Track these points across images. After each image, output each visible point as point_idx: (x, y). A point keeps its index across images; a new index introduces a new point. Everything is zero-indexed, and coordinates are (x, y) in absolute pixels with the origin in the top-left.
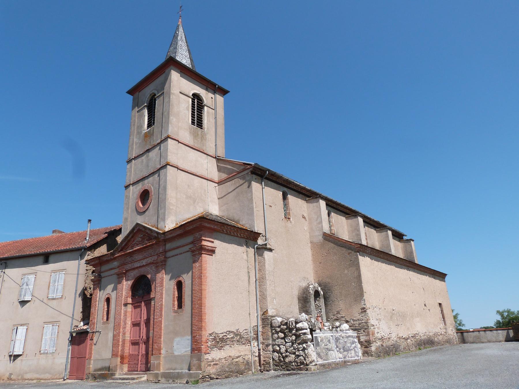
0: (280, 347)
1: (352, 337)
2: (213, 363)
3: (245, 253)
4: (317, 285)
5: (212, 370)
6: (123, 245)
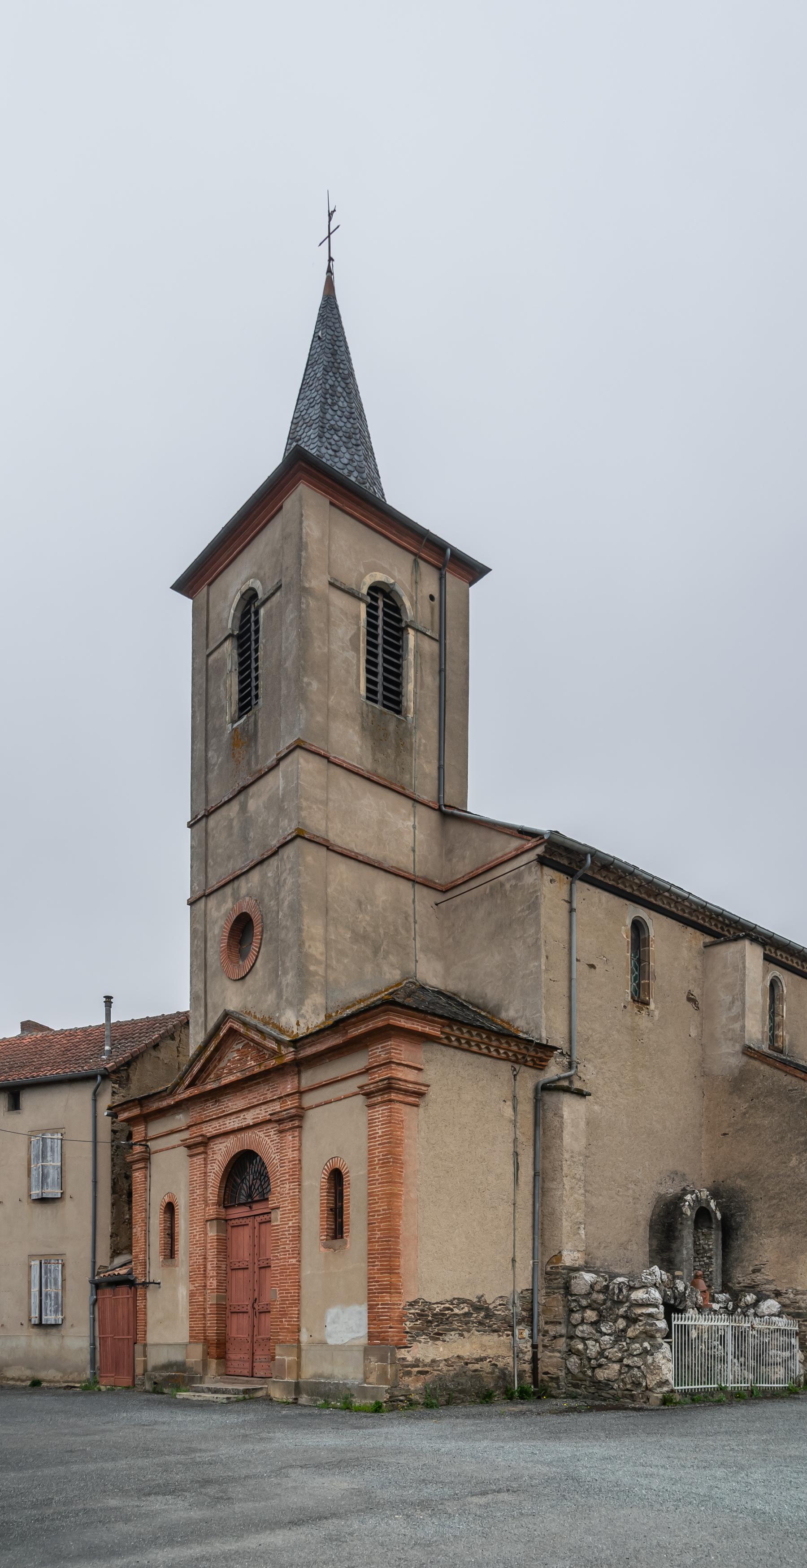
0: (585, 1344)
1: (784, 1332)
2: (417, 1369)
3: (509, 1103)
4: (705, 1194)
5: (414, 1385)
6: (196, 1070)
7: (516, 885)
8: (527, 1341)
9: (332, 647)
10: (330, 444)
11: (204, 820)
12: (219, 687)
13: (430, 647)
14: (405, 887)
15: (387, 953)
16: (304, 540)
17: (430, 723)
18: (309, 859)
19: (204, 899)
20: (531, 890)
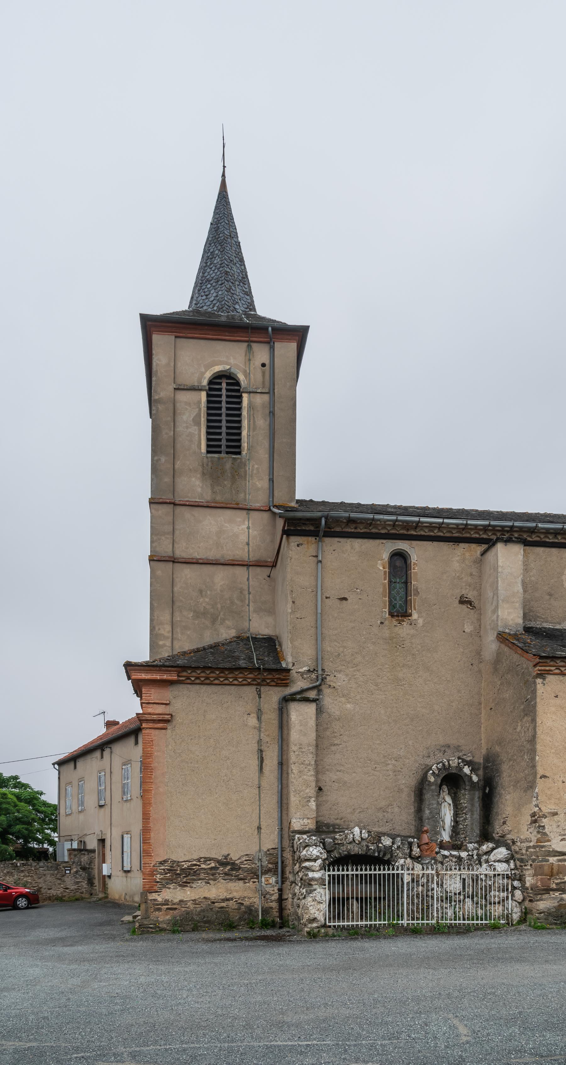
5: (163, 917)
8: (273, 886)
14: (240, 572)
15: (223, 620)
17: (262, 453)
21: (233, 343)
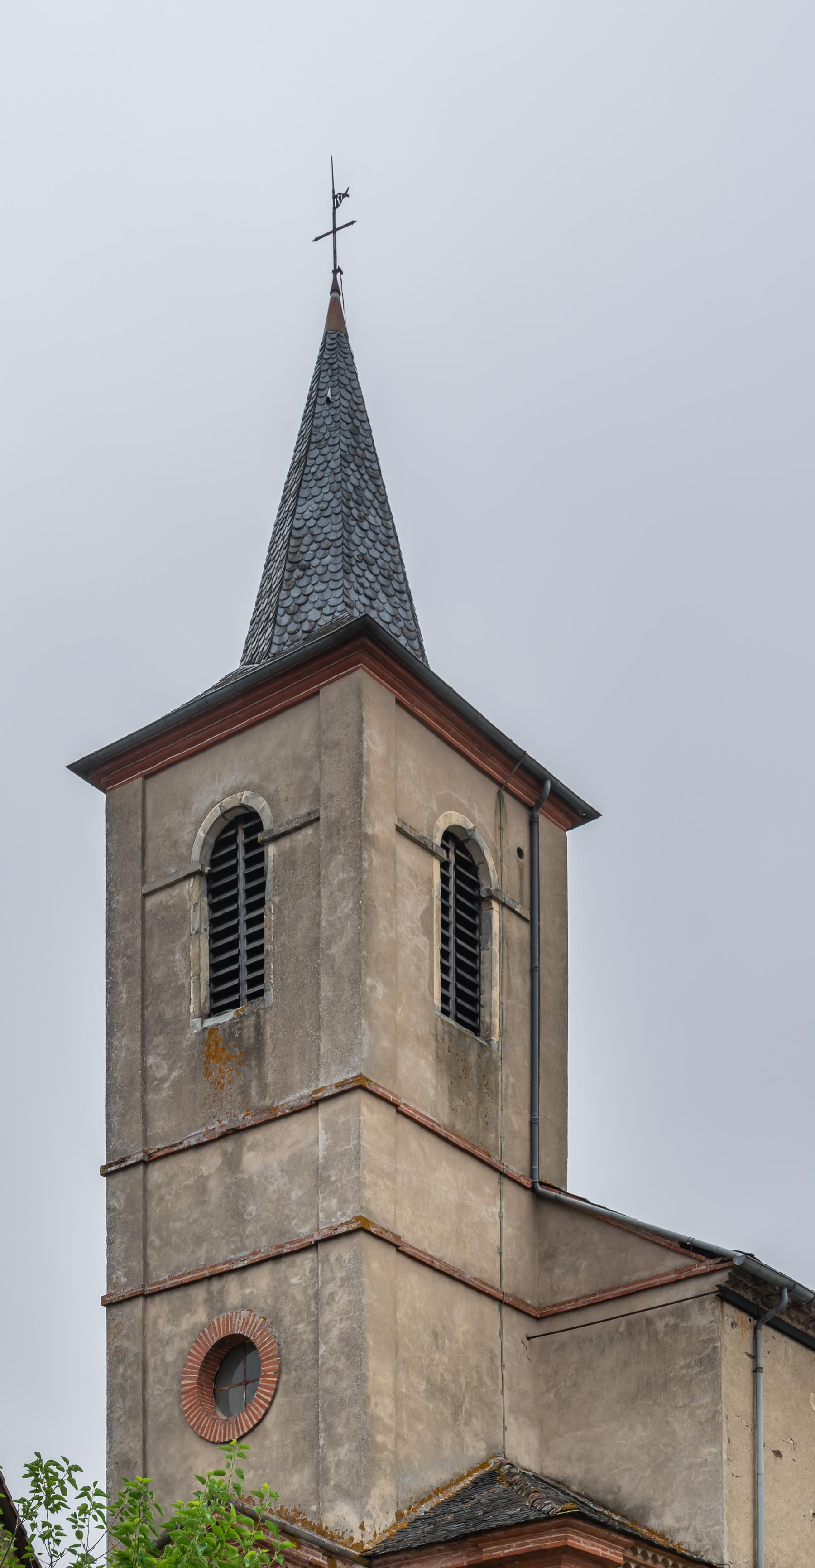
7: (676, 1326)
9: (399, 929)
10: (362, 585)
11: (141, 1168)
12: (172, 953)
13: (519, 931)
14: (489, 1308)
15: (470, 1415)
16: (365, 759)
18: (375, 1265)
19: (141, 1300)
20: (704, 1337)
21: (277, 719)
